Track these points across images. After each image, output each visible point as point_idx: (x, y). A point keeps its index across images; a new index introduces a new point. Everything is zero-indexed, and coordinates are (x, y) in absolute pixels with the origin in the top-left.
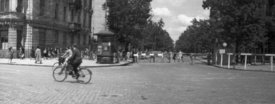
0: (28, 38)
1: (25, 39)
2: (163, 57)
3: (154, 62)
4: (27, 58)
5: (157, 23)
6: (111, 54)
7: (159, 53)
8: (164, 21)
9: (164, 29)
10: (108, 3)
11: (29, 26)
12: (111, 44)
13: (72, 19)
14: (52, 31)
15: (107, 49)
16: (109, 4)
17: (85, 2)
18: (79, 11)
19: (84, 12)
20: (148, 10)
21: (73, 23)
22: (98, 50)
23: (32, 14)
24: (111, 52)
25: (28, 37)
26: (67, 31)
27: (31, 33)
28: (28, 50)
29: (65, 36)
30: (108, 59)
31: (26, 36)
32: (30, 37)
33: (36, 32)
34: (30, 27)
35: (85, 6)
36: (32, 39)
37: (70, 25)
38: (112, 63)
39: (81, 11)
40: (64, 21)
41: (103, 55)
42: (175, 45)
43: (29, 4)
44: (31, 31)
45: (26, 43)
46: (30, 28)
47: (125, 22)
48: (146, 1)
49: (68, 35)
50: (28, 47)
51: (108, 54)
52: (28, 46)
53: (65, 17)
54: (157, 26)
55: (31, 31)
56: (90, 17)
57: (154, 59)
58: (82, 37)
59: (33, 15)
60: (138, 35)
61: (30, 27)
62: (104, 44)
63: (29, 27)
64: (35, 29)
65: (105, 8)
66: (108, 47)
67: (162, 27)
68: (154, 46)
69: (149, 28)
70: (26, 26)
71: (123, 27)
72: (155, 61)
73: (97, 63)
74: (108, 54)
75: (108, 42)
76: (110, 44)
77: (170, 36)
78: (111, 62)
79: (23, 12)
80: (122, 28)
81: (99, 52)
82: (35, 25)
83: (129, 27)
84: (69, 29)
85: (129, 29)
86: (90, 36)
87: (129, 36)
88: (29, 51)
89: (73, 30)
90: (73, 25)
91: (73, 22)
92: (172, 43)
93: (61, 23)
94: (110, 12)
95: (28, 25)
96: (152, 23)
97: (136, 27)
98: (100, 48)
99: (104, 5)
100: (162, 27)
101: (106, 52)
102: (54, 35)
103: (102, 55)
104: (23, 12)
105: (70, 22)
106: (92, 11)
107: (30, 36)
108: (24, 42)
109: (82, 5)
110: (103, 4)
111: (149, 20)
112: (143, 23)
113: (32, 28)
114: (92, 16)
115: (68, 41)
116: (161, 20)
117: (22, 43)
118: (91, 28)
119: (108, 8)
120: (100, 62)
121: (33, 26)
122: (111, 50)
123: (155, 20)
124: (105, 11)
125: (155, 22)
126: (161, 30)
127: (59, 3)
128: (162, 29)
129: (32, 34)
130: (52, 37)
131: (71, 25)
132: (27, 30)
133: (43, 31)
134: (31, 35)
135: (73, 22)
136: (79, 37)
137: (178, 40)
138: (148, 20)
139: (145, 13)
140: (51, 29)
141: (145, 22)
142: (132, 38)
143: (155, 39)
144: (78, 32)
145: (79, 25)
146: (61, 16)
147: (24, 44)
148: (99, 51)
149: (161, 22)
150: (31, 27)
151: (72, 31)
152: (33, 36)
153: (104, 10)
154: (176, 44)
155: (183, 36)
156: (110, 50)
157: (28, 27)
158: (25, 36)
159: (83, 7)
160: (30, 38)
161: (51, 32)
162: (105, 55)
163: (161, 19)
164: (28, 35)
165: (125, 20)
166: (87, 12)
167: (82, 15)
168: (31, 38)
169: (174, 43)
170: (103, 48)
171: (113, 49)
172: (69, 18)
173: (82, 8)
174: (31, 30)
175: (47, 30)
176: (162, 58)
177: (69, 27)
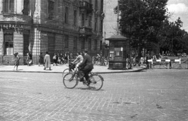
1: (33, 44)
2: (181, 63)
5: (174, 23)
8: (182, 20)
9: (182, 28)
10: (120, 6)
11: (37, 30)
12: (123, 49)
13: (83, 23)
15: (119, 54)
16: (121, 7)
17: (96, 2)
18: (89, 15)
21: (83, 28)
22: (110, 55)
27: (40, 37)
28: (36, 56)
30: (120, 64)
33: (45, 36)
34: (38, 31)
35: (96, 10)
36: (41, 44)
37: (81, 29)
38: (124, 69)
40: (75, 25)
41: (116, 61)
43: (36, 7)
44: (39, 36)
46: (38, 32)
49: (78, 40)
50: (36, 53)
51: (120, 59)
52: (35, 51)
53: (75, 21)
56: (102, 21)
58: (93, 42)
59: (41, 19)
61: (38, 31)
62: (116, 49)
64: (44, 34)
65: (117, 12)
66: (120, 52)
67: (179, 27)
70: (34, 30)
72: (172, 67)
74: (120, 59)
75: (120, 47)
76: (122, 49)
78: (124, 67)
79: (30, 15)
81: (111, 57)
82: (44, 29)
84: (80, 34)
86: (101, 41)
87: (143, 40)
90: (84, 30)
93: (71, 28)
95: (36, 29)
97: (151, 29)
98: (112, 54)
99: (116, 9)
101: (119, 58)
102: (64, 40)
103: (114, 61)
105: (81, 27)
106: (104, 15)
107: (39, 41)
108: (32, 47)
109: (93, 9)
113: (40, 32)
114: (104, 20)
115: (79, 47)
117: (29, 48)
119: (120, 11)
122: (124, 55)
124: (117, 14)
128: (180, 29)
129: (40, 39)
130: (62, 42)
133: (52, 35)
134: (40, 40)
135: (84, 27)
136: (90, 42)
139: (160, 15)
142: (145, 42)
146: (71, 21)
147: (32, 50)
148: (111, 56)
149: (179, 22)
150: (39, 32)
151: (82, 36)
152: (41, 41)
153: (116, 13)
156: (122, 55)
157: (35, 31)
158: (33, 41)
164: (35, 40)
166: (99, 16)
167: (93, 19)
170: (115, 53)
171: (126, 55)
172: (79, 23)
175: (57, 35)
177: (80, 32)
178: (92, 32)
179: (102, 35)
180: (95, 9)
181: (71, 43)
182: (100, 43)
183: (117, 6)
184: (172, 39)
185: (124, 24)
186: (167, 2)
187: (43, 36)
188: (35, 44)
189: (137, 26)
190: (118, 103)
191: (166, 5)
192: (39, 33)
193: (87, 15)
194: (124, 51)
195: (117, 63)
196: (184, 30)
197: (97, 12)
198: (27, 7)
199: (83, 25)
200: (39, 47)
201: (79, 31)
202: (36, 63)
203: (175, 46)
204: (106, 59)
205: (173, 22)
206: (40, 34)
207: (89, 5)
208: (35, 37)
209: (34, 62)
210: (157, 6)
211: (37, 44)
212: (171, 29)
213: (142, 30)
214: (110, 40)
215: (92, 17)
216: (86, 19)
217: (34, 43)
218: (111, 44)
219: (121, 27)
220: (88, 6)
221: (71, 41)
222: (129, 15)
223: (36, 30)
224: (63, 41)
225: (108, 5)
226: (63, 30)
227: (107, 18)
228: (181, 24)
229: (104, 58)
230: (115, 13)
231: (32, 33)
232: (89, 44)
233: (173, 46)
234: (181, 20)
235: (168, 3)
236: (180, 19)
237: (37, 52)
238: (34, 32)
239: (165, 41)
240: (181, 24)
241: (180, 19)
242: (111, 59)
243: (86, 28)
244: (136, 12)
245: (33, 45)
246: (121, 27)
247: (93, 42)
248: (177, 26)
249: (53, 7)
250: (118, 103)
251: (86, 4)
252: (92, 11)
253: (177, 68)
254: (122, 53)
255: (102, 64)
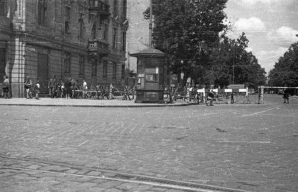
0: (18, 45)
1: (12, 64)
2: (249, 94)
3: (232, 103)
4: (17, 97)
5: (236, 41)
6: (159, 87)
7: (242, 88)
8: (247, 36)
9: (248, 50)
10: (153, 7)
11: (20, 41)
12: (160, 71)
13: (94, 35)
14: (60, 52)
15: (153, 78)
16: (156, 10)
17: (115, 3)
18: (105, 22)
19: (113, 25)
20: (222, 17)
21: (95, 42)
22: (138, 80)
23: (24, 21)
24: (160, 84)
25: (18, 61)
26: (85, 53)
27: (24, 53)
28: (18, 84)
29: (81, 63)
30: (155, 95)
31: (14, 59)
32: (21, 61)
33: (33, 52)
34: (21, 43)
35: (115, 16)
36: (25, 64)
37: (90, 45)
38: (161, 103)
39: (109, 21)
40: (81, 37)
41: (147, 89)
42: (267, 78)
43: (18, 4)
44: (22, 51)
45: (13, 71)
46: (21, 44)
47: (182, 38)
48: (217, 2)
49: (86, 61)
50: (17, 79)
51: (156, 86)
52: (17, 75)
53: (82, 29)
54: (236, 45)
55: (22, 51)
56: (124, 34)
57: (232, 98)
58: (110, 68)
59: (26, 23)
60: (205, 60)
61: (21, 43)
62: (147, 70)
63: (19, 44)
64: (31, 48)
65: (148, 16)
66: (155, 75)
67: (244, 47)
68: (232, 80)
69: (222, 50)
70: (15, 41)
71: (179, 47)
72: (234, 101)
73: (136, 102)
74: (156, 86)
75: (154, 67)
76: (157, 71)
77: (259, 63)
78: (160, 100)
79: (8, 15)
80: (177, 49)
81: (140, 84)
82: (30, 40)
83: (189, 47)
84: (89, 52)
85: (189, 49)
86: (123, 66)
87: (190, 62)
88: (19, 85)
89: (95, 54)
90: (95, 44)
91: (95, 40)
92: (263, 76)
93: (75, 41)
94: (158, 23)
95: (17, 39)
96: (227, 41)
97: (201, 47)
98: (141, 78)
99: (147, 12)
100: (244, 47)
101: (152, 84)
102: (63, 60)
103: (145, 89)
104: (8, 15)
105: (91, 40)
106: (127, 23)
107: (22, 60)
108: (11, 69)
109: (111, 12)
110: (145, 9)
111: (223, 36)
112: (212, 40)
113: (24, 45)
114: (127, 32)
115: (88, 71)
116: (243, 36)
117: (7, 70)
118: (125, 52)
119: (153, 16)
120: (141, 101)
121: (26, 42)
122: (160, 80)
123: (232, 35)
124: (148, 20)
125: (232, 39)
126: (244, 52)
127: (72, 6)
128: (245, 51)
129: (24, 56)
130: (60, 63)
131: (92, 44)
132: (15, 48)
133: (45, 52)
134: (23, 58)
135: (95, 40)
136: (105, 66)
137: (274, 70)
138: (220, 34)
139: (216, 23)
140: (58, 50)
141: (216, 38)
142: (193, 65)
143: (234, 68)
144: (104, 58)
145: (106, 45)
146: (74, 29)
147: (10, 73)
148: (139, 82)
149: (243, 39)
150: (22, 44)
151: (93, 54)
152: (26, 60)
153: (148, 19)
154: (269, 76)
155: (283, 63)
156: (158, 80)
157: (17, 43)
158: (12, 59)
159: (112, 16)
160: (20, 72)
161: (60, 55)
162: (150, 89)
163: (244, 34)
164: (17, 57)
165: (182, 36)
166: (119, 25)
167: (110, 29)
168: (24, 62)
169: (267, 75)
170: (146, 78)
171: (163, 79)
172: (88, 32)
173: (110, 18)
174: (22, 71)
175: (52, 51)
176: (247, 97)
177: (89, 48)
178: (109, 49)
179: (125, 56)
180: (113, 13)
181: (76, 62)
182: (121, 67)
183: (149, 9)
184: (233, 66)
185: (159, 35)
186: (226, 3)
187: (30, 52)
188: (16, 64)
189: (180, 39)
190: (155, 127)
191: (224, 7)
192: (22, 46)
193: (101, 23)
194: (161, 74)
195: (150, 93)
196: (251, 53)
197: (116, 19)
198: (4, 11)
199: (95, 38)
200: (22, 69)
201: (88, 47)
202: (18, 96)
203: (236, 76)
204: (131, 90)
205: (234, 40)
206: (24, 48)
207: (104, 6)
208: (17, 53)
209: (15, 93)
210: (210, 9)
211: (19, 73)
212: (232, 49)
213: (187, 46)
214: (138, 56)
215: (108, 26)
216: (99, 27)
217: (14, 57)
218: (140, 61)
219: (155, 41)
220: (102, 7)
221: (75, 62)
222: (168, 22)
223: (17, 42)
224: (62, 62)
225: (133, 10)
226: (62, 43)
227: (132, 31)
228: (246, 42)
229: (129, 87)
230: (145, 18)
231: (11, 45)
232: (104, 68)
233: (234, 77)
234: (245, 37)
235: (227, 4)
236: (244, 36)
237: (19, 78)
238: (15, 44)
239: (223, 71)
240: (246, 42)
241: (244, 36)
242: (139, 88)
243: (99, 43)
244: (179, 16)
245: (13, 66)
246: (155, 41)
247: (111, 66)
248: (241, 46)
249: (45, 6)
250: (155, 127)
251: (98, 5)
252: (108, 15)
253: (242, 102)
254: (158, 76)
255: (126, 97)
